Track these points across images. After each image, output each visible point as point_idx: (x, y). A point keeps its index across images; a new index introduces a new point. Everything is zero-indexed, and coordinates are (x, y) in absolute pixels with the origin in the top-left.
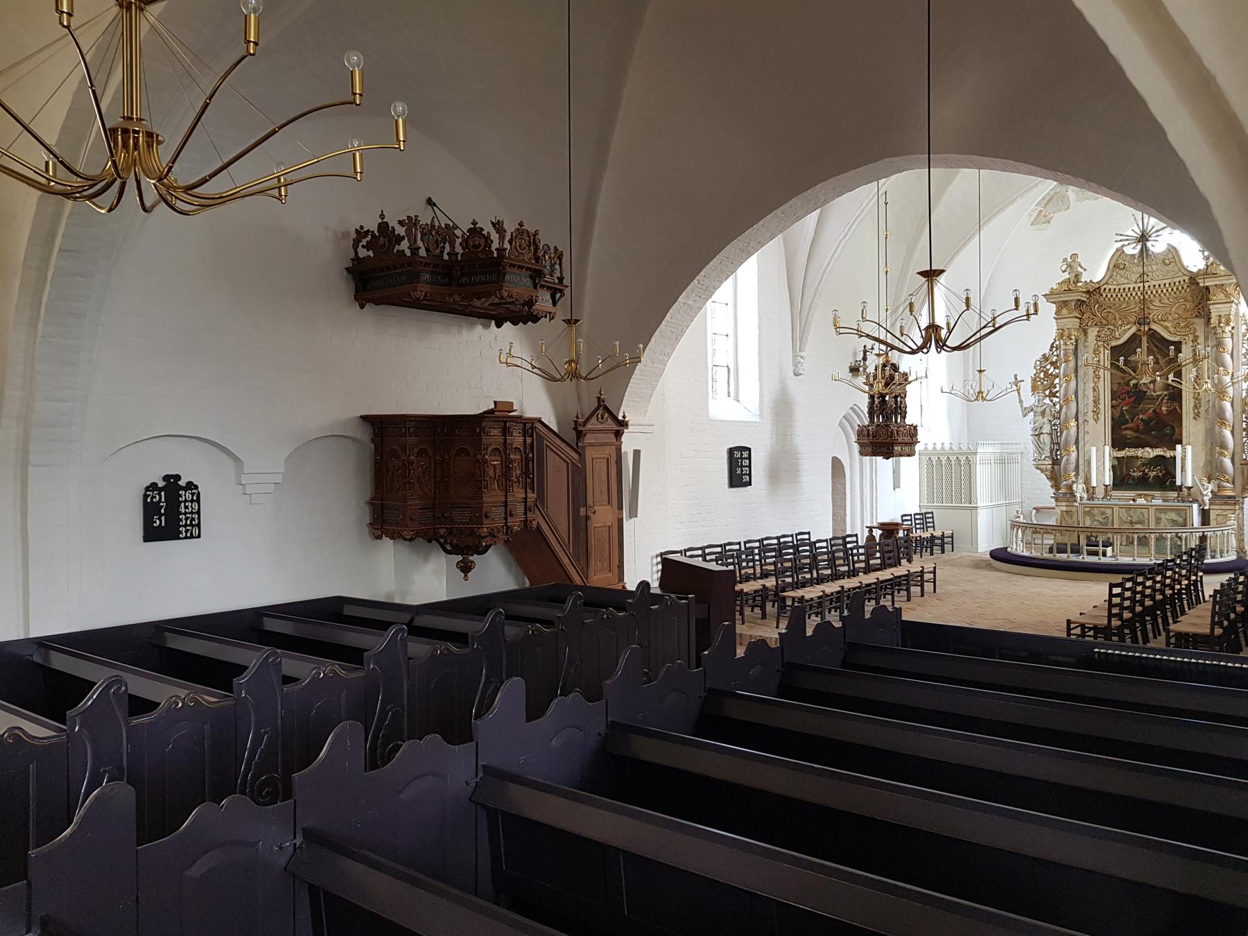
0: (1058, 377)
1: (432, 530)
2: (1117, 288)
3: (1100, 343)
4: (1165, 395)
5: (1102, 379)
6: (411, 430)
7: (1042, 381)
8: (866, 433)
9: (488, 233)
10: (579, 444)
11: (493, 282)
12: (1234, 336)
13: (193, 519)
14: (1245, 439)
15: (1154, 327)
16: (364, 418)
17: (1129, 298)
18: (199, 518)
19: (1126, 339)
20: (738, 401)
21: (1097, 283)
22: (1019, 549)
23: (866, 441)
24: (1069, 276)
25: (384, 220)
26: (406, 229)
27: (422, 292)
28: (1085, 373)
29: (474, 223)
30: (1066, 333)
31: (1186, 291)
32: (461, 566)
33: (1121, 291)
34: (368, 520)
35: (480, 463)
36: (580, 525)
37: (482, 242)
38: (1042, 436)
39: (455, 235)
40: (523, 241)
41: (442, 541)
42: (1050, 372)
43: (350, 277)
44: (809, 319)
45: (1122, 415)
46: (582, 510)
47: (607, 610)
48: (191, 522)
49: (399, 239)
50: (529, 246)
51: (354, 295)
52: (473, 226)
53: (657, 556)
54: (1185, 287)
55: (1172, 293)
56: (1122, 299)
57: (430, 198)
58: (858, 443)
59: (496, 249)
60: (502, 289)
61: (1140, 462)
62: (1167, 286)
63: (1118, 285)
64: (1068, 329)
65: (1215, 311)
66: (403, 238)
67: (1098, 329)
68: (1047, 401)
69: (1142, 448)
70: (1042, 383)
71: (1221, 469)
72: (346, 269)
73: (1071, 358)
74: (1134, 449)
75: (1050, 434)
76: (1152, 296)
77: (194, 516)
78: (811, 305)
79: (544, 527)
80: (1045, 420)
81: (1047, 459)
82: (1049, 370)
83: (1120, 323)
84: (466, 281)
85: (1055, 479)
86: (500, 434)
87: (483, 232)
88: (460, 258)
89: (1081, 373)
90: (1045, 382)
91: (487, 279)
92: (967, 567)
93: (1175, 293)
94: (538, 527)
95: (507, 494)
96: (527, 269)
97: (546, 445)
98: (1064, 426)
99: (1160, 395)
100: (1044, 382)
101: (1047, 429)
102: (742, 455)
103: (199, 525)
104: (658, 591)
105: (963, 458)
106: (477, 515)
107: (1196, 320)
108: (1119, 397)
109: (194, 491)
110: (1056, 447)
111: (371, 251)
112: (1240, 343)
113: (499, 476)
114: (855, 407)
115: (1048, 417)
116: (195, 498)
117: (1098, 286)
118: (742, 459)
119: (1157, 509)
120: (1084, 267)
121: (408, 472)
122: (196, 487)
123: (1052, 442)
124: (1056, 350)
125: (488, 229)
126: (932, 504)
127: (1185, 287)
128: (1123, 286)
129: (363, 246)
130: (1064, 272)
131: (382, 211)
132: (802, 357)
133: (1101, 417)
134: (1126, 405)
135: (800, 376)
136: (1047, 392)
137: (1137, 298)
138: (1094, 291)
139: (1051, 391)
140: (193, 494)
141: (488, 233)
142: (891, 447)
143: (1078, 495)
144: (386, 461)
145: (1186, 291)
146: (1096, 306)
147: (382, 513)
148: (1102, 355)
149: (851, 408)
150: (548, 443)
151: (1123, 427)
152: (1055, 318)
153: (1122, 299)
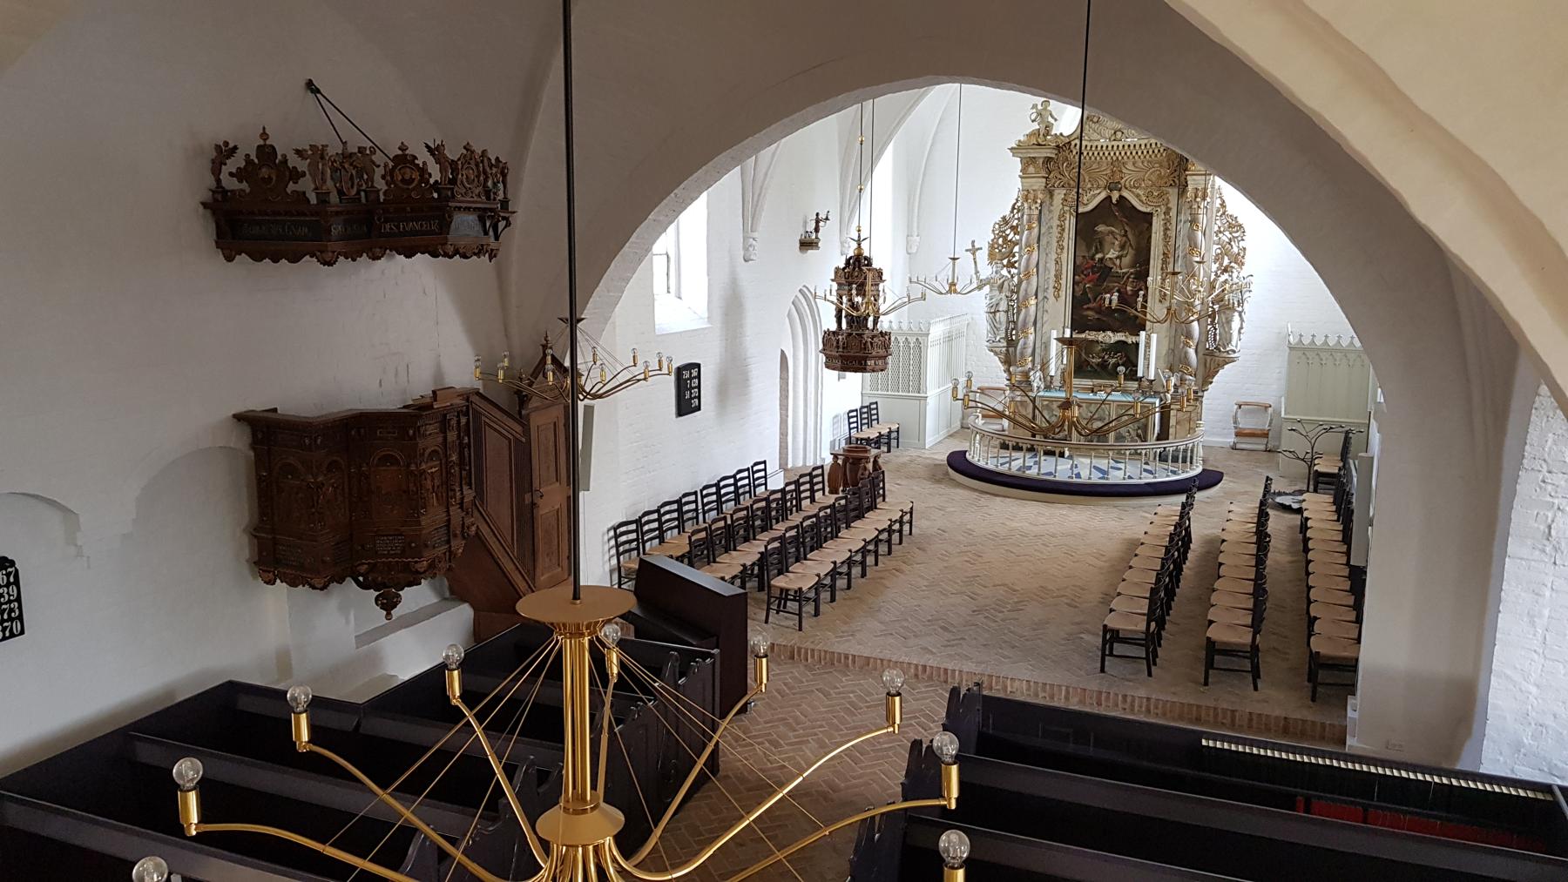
0: (1017, 244)
1: (349, 569)
2: (1089, 144)
3: (1066, 208)
4: (1132, 274)
5: (1065, 250)
7: (1000, 248)
8: (835, 344)
9: (424, 163)
10: (523, 412)
11: (432, 233)
12: (1209, 211)
13: (12, 610)
14: (1209, 327)
15: (1125, 194)
17: (1101, 158)
18: (20, 607)
19: (1095, 205)
20: (680, 298)
21: (1068, 136)
22: (981, 457)
23: (834, 353)
24: (1038, 127)
25: (268, 142)
26: (309, 164)
27: (334, 252)
28: (1048, 242)
29: (403, 148)
30: (1031, 196)
31: (1162, 155)
32: (382, 604)
33: (1093, 149)
34: (246, 553)
35: (416, 475)
36: (526, 516)
37: (416, 175)
38: (998, 314)
39: (374, 163)
40: (471, 171)
42: (1009, 238)
43: (208, 212)
44: (764, 191)
45: (1084, 293)
46: (527, 497)
47: (637, 707)
48: (9, 614)
49: (296, 175)
50: (478, 176)
52: (400, 152)
53: (609, 530)
54: (1162, 150)
55: (1148, 157)
56: (1093, 158)
57: (310, 80)
58: (826, 355)
61: (1100, 348)
62: (1143, 147)
63: (1090, 140)
64: (1034, 191)
65: (1193, 182)
66: (303, 174)
67: (1065, 191)
68: (1004, 272)
69: (1104, 332)
70: (1000, 251)
71: (1185, 360)
73: (1034, 225)
74: (1094, 333)
75: (1007, 312)
76: (1125, 157)
77: (12, 606)
78: (766, 174)
79: (485, 530)
80: (1003, 295)
81: (1002, 340)
82: (1008, 235)
83: (1089, 186)
84: (391, 229)
85: (1008, 361)
86: (437, 431)
87: (416, 162)
88: (382, 198)
89: (1044, 241)
90: (1004, 250)
91: (424, 228)
92: (924, 479)
93: (1150, 156)
94: (477, 533)
95: (448, 508)
96: (475, 209)
97: (485, 422)
98: (1022, 304)
99: (1126, 273)
100: (1002, 251)
101: (1003, 306)
102: (691, 374)
103: (20, 618)
105: (912, 340)
106: (413, 545)
107: (1170, 190)
108: (1082, 272)
109: (9, 570)
110: (1012, 326)
112: (1214, 219)
113: (438, 487)
114: (805, 289)
115: (1006, 292)
116: (12, 580)
117: (1068, 141)
118: (691, 378)
119: (1118, 405)
120: (1056, 117)
122: (12, 563)
123: (1008, 322)
124: (1017, 213)
125: (423, 157)
126: (876, 392)
127: (1162, 150)
128: (1096, 143)
130: (1033, 121)
131: (264, 128)
132: (754, 239)
133: (1062, 293)
134: (1089, 282)
135: (750, 262)
136: (1005, 262)
137: (1109, 158)
138: (1063, 146)
139: (1009, 261)
140: (8, 575)
141: (424, 163)
142: (863, 362)
143: (1035, 385)
145: (1162, 155)
146: (1065, 165)
148: (1067, 222)
149: (800, 291)
150: (487, 421)
151: (1085, 307)
152: (1020, 177)
153: (1093, 158)
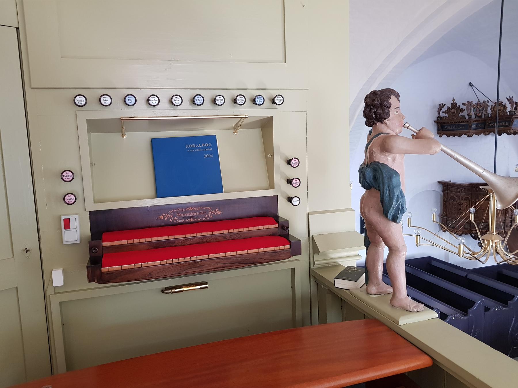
6: (462, 190)
16: (439, 182)
25: (454, 102)
37: (502, 108)
39: (488, 105)
41: (473, 235)
43: (436, 124)
49: (462, 111)
51: (437, 132)
59: (509, 111)
60: (511, 129)
72: (434, 121)
84: (492, 125)
87: (502, 104)
104: (460, 116)
111: (447, 114)
121: (460, 207)
129: (443, 112)
144: (449, 201)
147: (447, 222)
